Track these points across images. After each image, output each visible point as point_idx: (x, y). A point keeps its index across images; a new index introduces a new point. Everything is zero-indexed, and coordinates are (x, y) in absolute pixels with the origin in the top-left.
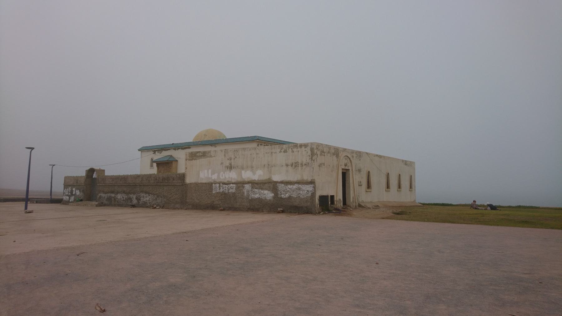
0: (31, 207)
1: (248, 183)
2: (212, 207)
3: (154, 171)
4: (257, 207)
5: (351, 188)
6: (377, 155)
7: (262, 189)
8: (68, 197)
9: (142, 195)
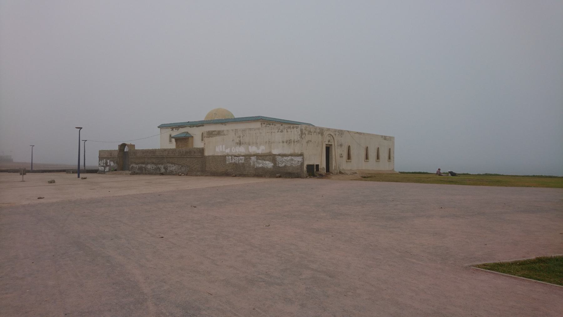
0: (82, 175)
1: (254, 155)
2: (226, 174)
3: (173, 145)
4: (260, 173)
5: (334, 159)
6: (357, 133)
7: (264, 160)
8: (103, 168)
9: (169, 165)
